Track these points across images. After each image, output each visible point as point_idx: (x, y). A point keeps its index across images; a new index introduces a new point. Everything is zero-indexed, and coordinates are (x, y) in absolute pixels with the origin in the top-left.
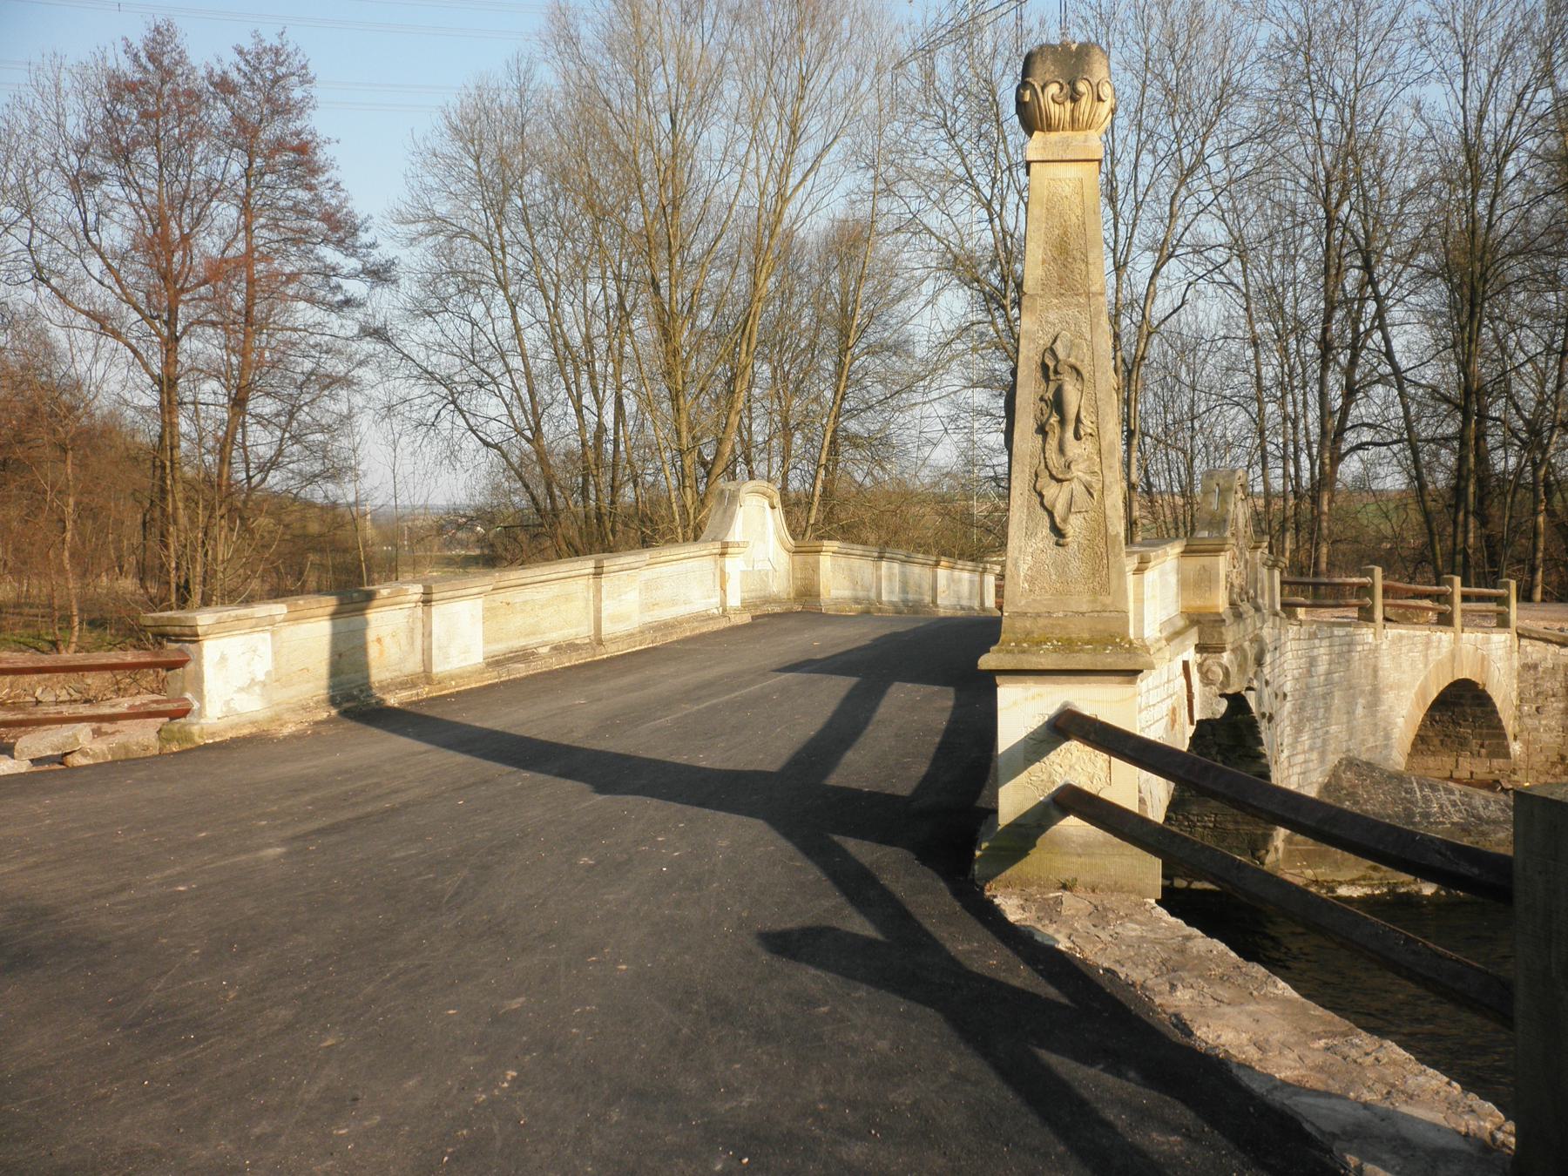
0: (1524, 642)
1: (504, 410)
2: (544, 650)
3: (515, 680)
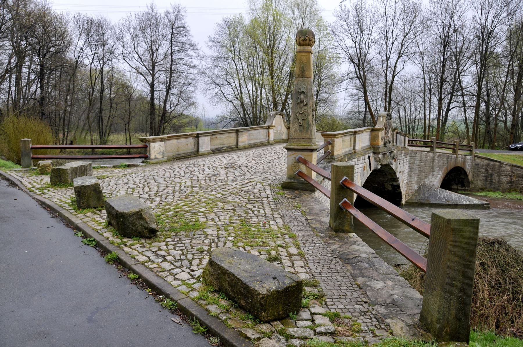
0: (476, 158)
1: (232, 92)
2: (225, 148)
3: (471, 205)
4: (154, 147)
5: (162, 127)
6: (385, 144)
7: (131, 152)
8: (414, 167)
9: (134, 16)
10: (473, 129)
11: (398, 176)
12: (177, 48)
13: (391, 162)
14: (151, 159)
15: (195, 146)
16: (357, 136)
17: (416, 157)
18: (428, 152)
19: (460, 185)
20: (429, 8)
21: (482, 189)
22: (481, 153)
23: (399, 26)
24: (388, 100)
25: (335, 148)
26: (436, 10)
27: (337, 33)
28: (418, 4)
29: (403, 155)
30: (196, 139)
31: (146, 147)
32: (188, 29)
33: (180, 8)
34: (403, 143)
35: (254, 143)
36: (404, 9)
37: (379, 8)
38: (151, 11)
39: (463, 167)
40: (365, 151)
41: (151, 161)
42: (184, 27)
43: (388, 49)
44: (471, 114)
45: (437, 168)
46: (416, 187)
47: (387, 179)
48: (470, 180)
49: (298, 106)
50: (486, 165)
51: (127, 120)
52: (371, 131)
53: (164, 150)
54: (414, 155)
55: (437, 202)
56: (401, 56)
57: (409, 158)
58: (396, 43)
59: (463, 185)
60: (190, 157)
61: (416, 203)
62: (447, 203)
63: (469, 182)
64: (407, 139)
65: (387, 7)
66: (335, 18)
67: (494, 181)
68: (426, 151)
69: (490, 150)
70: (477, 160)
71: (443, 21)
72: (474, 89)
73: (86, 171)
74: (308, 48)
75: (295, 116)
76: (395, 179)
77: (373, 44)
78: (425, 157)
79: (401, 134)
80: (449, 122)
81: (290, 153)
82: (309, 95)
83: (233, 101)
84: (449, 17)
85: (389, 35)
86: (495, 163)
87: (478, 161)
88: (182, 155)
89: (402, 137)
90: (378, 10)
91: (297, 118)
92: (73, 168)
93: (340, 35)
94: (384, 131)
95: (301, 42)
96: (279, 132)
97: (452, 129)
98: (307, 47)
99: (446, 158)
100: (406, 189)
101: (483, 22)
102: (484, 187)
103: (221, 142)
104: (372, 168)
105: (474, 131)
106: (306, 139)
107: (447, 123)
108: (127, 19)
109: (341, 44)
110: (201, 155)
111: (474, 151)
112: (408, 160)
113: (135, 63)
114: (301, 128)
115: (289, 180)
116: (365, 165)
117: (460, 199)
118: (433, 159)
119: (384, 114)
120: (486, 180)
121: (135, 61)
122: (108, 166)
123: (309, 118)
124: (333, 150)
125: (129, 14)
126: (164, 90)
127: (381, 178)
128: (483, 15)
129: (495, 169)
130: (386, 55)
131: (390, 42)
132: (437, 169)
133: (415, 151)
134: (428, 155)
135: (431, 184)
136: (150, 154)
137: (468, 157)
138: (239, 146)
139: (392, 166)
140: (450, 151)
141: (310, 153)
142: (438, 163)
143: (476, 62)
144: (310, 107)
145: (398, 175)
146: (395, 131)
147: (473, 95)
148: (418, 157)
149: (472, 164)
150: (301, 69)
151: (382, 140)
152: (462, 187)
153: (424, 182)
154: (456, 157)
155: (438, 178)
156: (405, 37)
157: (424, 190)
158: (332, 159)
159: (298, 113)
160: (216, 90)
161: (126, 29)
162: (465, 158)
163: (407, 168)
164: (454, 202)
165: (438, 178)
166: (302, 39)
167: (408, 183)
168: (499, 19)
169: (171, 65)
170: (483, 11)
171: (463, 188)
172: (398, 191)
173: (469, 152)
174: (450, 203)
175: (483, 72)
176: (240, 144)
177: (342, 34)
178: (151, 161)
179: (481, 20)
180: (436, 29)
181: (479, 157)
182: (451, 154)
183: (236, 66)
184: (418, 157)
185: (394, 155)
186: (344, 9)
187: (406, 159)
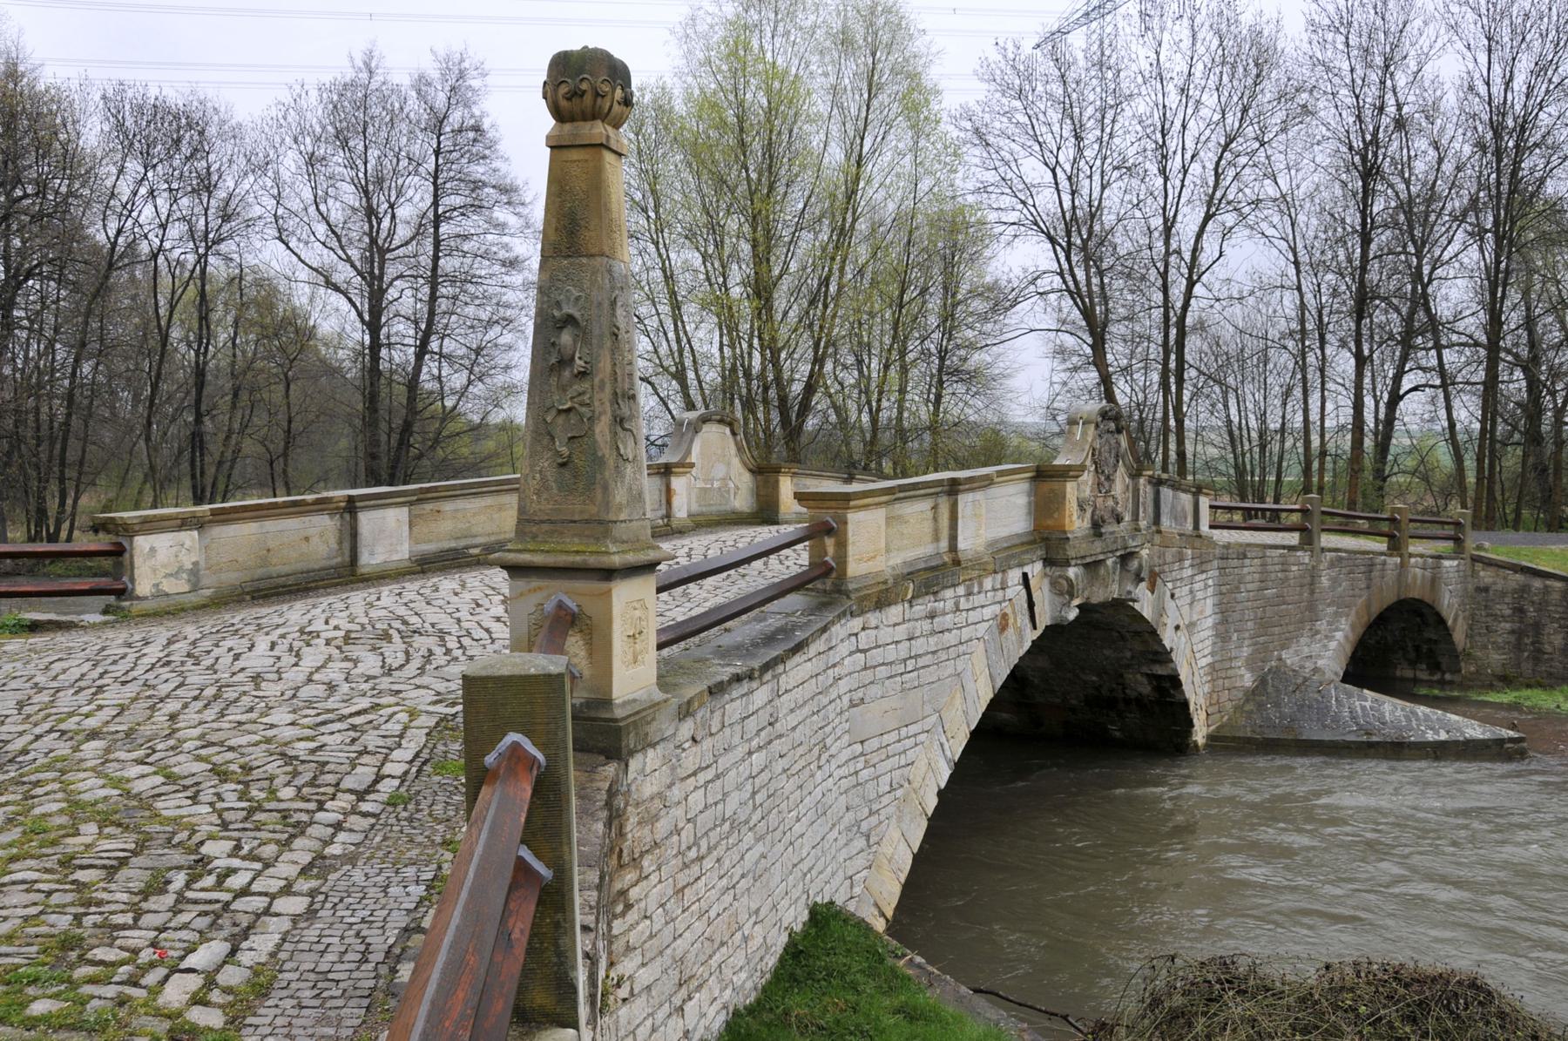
0: (1479, 566)
2: (476, 551)
3: (1456, 742)
4: (153, 550)
6: (1097, 525)
8: (1239, 607)
9: (314, 94)
10: (1478, 460)
11: (1167, 643)
13: (1129, 593)
14: (138, 598)
15: (340, 543)
16: (965, 500)
17: (1246, 570)
18: (1291, 548)
19: (1424, 666)
20: (1305, 46)
21: (1506, 680)
22: (1497, 546)
23: (1205, 112)
24: (1173, 365)
25: (851, 550)
26: (1329, 53)
27: (991, 139)
28: (1266, 33)
29: (1187, 563)
30: (347, 516)
31: (118, 552)
33: (466, 65)
34: (1190, 520)
36: (1220, 52)
37: (1133, 49)
38: (364, 75)
39: (1427, 599)
40: (1004, 556)
41: (137, 607)
42: (477, 129)
43: (1170, 191)
44: (1467, 412)
45: (1329, 605)
46: (1248, 680)
47: (1128, 654)
48: (1460, 648)
49: (553, 380)
50: (1515, 591)
52: (1033, 479)
53: (196, 564)
54: (1235, 563)
55: (1327, 736)
56: (1214, 214)
57: (1216, 573)
58: (1195, 168)
59: (1435, 667)
60: (317, 588)
61: (1249, 740)
62: (1365, 738)
63: (1455, 655)
64: (1204, 502)
65: (1165, 46)
66: (985, 86)
67: (1548, 648)
68: (1284, 547)
69: (1543, 535)
70: (1482, 574)
71: (1357, 92)
72: (1474, 324)
74: (599, 130)
76: (1156, 653)
77: (1116, 174)
78: (1277, 568)
79: (1176, 487)
80: (1399, 441)
81: (522, 584)
82: (596, 332)
83: (653, 379)
84: (1374, 77)
85: (1173, 144)
86: (1548, 582)
87: (1486, 576)
89: (1186, 499)
90: (1134, 56)
93: (1001, 144)
94: (1088, 478)
95: (564, 103)
96: (716, 485)
97: (1410, 463)
98: (588, 125)
99: (1362, 569)
100: (1207, 688)
101: (1494, 90)
102: (1511, 672)
103: (460, 526)
104: (1044, 620)
105: (1480, 469)
106: (587, 522)
107: (1394, 441)
108: (293, 105)
109: (1008, 177)
110: (367, 580)
111: (1472, 540)
112: (1210, 582)
114: (567, 474)
116: (1009, 611)
117: (1414, 723)
118: (1313, 574)
119: (1090, 413)
120: (1518, 647)
122: (52, 616)
123: (597, 430)
124: (842, 558)
125: (298, 89)
126: (411, 341)
127: (1107, 652)
128: (1497, 69)
129: (1547, 603)
130: (1164, 209)
131: (1175, 164)
132: (1330, 610)
133: (1241, 545)
134: (1292, 560)
135: (1309, 665)
136: (132, 580)
137: (1447, 563)
139: (1137, 606)
140: (1380, 545)
141: (603, 586)
142: (1333, 588)
143: (1478, 234)
144: (602, 381)
145: (1168, 638)
146: (1140, 475)
147: (1477, 344)
148: (1250, 568)
149: (1466, 589)
151: (1082, 508)
152: (1431, 674)
153: (1280, 659)
154: (1402, 565)
155: (1333, 645)
156: (1226, 148)
157: (1278, 691)
158: (839, 592)
159: (554, 412)
161: (288, 140)
162: (1439, 567)
163: (1209, 610)
164: (1390, 734)
165: (1333, 645)
166: (563, 89)
167: (1217, 666)
168: (1550, 81)
169: (436, 258)
170: (1494, 57)
171: (1436, 677)
172: (1173, 696)
173: (1450, 544)
174: (1375, 739)
175: (1503, 265)
177: (1007, 141)
178: (137, 607)
179: (1488, 84)
180: (1333, 117)
181: (1489, 563)
182: (1382, 554)
184: (1250, 568)
185: (1141, 566)
186: (1012, 56)
187: (1204, 576)
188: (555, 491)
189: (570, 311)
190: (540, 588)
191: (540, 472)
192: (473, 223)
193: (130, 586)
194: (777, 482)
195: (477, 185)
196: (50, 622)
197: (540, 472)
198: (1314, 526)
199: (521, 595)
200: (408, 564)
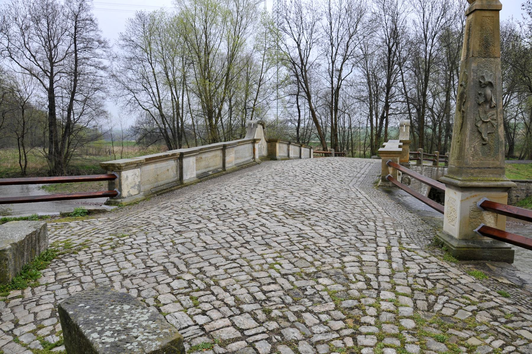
2: (210, 173)
4: (127, 177)
5: (67, 140)
7: (27, 173)
12: (81, 45)
14: (123, 198)
15: (177, 171)
30: (178, 160)
32: (96, 22)
35: (240, 163)
41: (125, 202)
49: (481, 109)
51: (20, 133)
73: (39, 242)
75: (475, 128)
81: (467, 194)
88: (162, 188)
91: (479, 131)
92: (15, 244)
103: (207, 163)
106: (495, 168)
113: (26, 62)
114: (486, 148)
115: (463, 244)
119: (407, 123)
121: (26, 60)
123: (499, 130)
136: (120, 190)
138: (227, 169)
150: (484, 43)
154: (438, 170)
159: (481, 122)
160: (129, 97)
169: (76, 66)
176: (227, 165)
183: (153, 69)
188: (481, 155)
189: (490, 80)
190: (476, 196)
191: (474, 147)
192: (87, 55)
193: (119, 193)
194: (276, 145)
195: (90, 40)
196: (95, 210)
197: (474, 147)
198: (421, 158)
199: (467, 198)
200: (196, 179)
